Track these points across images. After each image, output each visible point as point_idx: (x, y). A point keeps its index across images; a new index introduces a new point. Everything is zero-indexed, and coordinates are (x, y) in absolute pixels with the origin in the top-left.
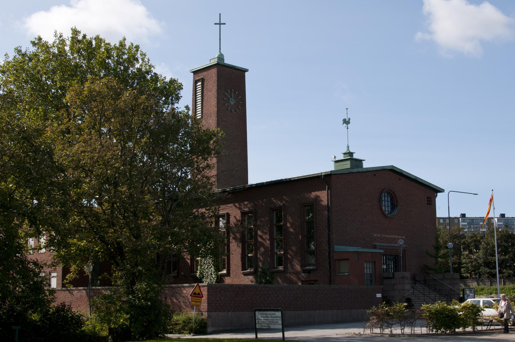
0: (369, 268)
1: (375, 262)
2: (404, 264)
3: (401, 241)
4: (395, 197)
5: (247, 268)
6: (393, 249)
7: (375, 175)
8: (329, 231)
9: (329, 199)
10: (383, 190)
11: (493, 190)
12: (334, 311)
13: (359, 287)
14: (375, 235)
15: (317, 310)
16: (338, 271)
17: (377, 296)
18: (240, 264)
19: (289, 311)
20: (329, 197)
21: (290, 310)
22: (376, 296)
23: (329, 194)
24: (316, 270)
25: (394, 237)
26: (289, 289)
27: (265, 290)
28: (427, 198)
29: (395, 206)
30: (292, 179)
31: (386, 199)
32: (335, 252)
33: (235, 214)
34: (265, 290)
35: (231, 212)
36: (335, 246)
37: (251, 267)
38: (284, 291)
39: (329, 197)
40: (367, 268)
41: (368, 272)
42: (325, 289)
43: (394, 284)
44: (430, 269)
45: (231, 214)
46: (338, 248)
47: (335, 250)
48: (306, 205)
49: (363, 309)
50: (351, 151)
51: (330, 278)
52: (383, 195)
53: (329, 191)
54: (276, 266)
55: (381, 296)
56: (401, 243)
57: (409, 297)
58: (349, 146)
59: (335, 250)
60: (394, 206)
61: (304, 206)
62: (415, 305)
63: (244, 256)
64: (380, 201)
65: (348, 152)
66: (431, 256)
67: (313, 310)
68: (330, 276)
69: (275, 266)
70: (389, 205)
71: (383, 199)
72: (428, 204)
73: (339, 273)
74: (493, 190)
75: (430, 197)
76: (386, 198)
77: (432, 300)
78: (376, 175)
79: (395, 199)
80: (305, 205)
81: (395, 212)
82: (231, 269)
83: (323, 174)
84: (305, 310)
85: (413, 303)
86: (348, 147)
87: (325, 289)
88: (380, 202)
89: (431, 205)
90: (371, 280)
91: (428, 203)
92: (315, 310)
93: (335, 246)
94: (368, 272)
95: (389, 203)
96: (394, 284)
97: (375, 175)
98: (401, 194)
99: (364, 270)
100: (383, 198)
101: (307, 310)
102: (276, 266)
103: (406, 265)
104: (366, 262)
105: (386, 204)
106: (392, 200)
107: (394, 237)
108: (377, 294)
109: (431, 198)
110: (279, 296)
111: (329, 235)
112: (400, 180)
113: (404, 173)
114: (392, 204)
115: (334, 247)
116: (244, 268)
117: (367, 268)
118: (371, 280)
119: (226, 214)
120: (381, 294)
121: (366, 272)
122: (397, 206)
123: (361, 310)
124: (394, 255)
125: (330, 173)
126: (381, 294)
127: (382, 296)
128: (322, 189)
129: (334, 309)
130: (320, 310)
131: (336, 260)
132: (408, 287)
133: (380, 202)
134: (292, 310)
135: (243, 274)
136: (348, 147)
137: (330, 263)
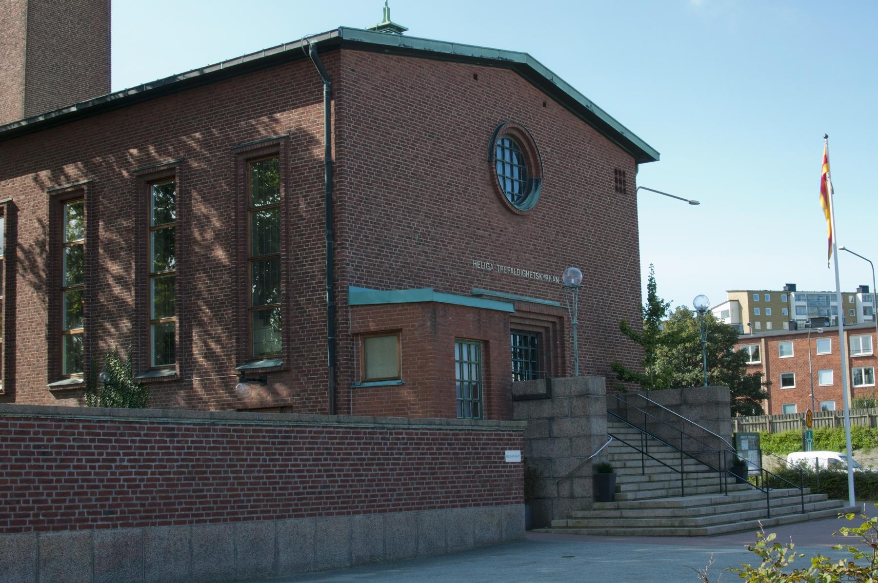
0: (469, 364)
1: (486, 343)
2: (560, 360)
3: (574, 272)
4: (533, 152)
5: (64, 373)
6: (530, 312)
7: (475, 77)
8: (332, 237)
9: (333, 128)
10: (498, 130)
11: (826, 137)
12: (358, 517)
13: (448, 424)
14: (477, 264)
15: (290, 516)
16: (361, 374)
17: (507, 460)
18: (44, 362)
19: (165, 527)
20: (333, 123)
21: (169, 523)
22: (504, 458)
23: (333, 110)
24: (287, 370)
25: (529, 274)
26: (165, 429)
27: (44, 433)
28: (616, 171)
29: (531, 180)
30: (207, 71)
31: (507, 159)
32: (353, 306)
33: (32, 204)
34: (44, 433)
35: (22, 197)
36: (353, 289)
37: (76, 365)
38: (139, 435)
39: (333, 123)
40: (461, 363)
41: (466, 377)
42: (322, 432)
43: (551, 419)
44: (630, 380)
45: (19, 205)
46: (358, 295)
47: (352, 301)
48: (255, 154)
49: (462, 506)
50: (396, 20)
51: (335, 401)
52: (499, 142)
53: (333, 103)
54: (153, 365)
55: (519, 459)
56: (573, 281)
57: (605, 460)
58: (389, 9)
59: (352, 301)
60: (528, 183)
61: (248, 160)
62: (623, 488)
63: (55, 334)
64: (491, 160)
65: (387, 22)
66: (635, 338)
67: (271, 518)
68: (335, 392)
69: (150, 364)
70: (516, 176)
71: (499, 157)
72: (617, 189)
73: (363, 382)
74: (826, 137)
75: (622, 169)
76: (507, 153)
77: (669, 470)
78: (479, 77)
79: (532, 160)
80: (250, 155)
81: (534, 199)
82: (17, 376)
83: (313, 41)
84: (238, 519)
85: (618, 480)
86: (387, 11)
87: (322, 432)
88: (490, 161)
89: (625, 193)
90: (475, 404)
91: (616, 187)
92: (278, 517)
93: (353, 289)
94: (466, 377)
95: (516, 170)
96: (551, 419)
97: (475, 77)
98: (548, 150)
99: (454, 368)
100: (499, 152)
101: (245, 519)
102: (153, 365)
103: (564, 363)
104: (460, 340)
105: (508, 174)
106: (523, 165)
107: (529, 274)
108: (507, 453)
109: (624, 173)
110: (114, 461)
111: (331, 250)
112: (544, 105)
113: (559, 85)
114: (522, 174)
115: (347, 292)
116: (55, 374)
117: (461, 363)
118: (475, 404)
119: (5, 206)
120: (518, 452)
121: (458, 377)
122: (538, 182)
123: (455, 510)
124: (529, 332)
125: (335, 35)
126: (518, 452)
127: (525, 460)
128: (309, 99)
129: (358, 513)
130: (302, 516)
131: (356, 335)
132: (600, 426)
133: (490, 161)
134: (176, 523)
135: (52, 392)
136: (387, 11)
137: (333, 345)
